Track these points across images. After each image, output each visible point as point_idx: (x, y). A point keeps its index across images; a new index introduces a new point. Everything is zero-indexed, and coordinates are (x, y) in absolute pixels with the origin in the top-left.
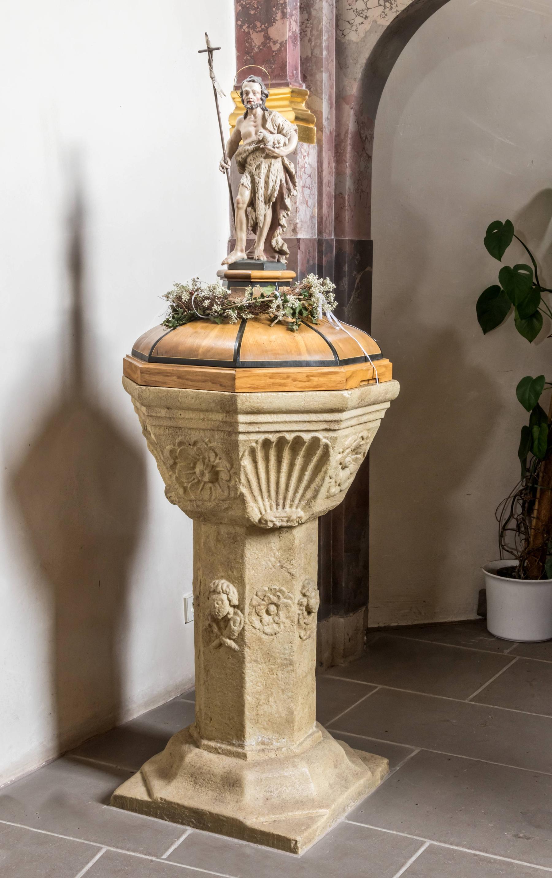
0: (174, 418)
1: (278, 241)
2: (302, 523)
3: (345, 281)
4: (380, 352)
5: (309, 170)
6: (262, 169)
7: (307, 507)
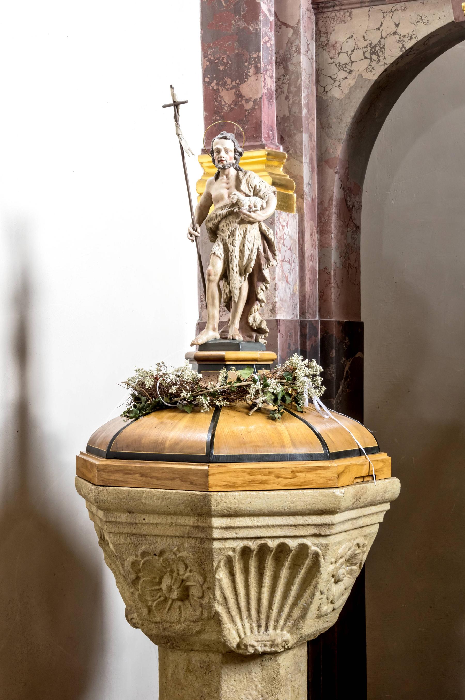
0: (136, 523)
1: (257, 317)
2: (289, 649)
3: (333, 368)
4: (376, 445)
5: (288, 243)
6: (237, 236)
7: (294, 628)
